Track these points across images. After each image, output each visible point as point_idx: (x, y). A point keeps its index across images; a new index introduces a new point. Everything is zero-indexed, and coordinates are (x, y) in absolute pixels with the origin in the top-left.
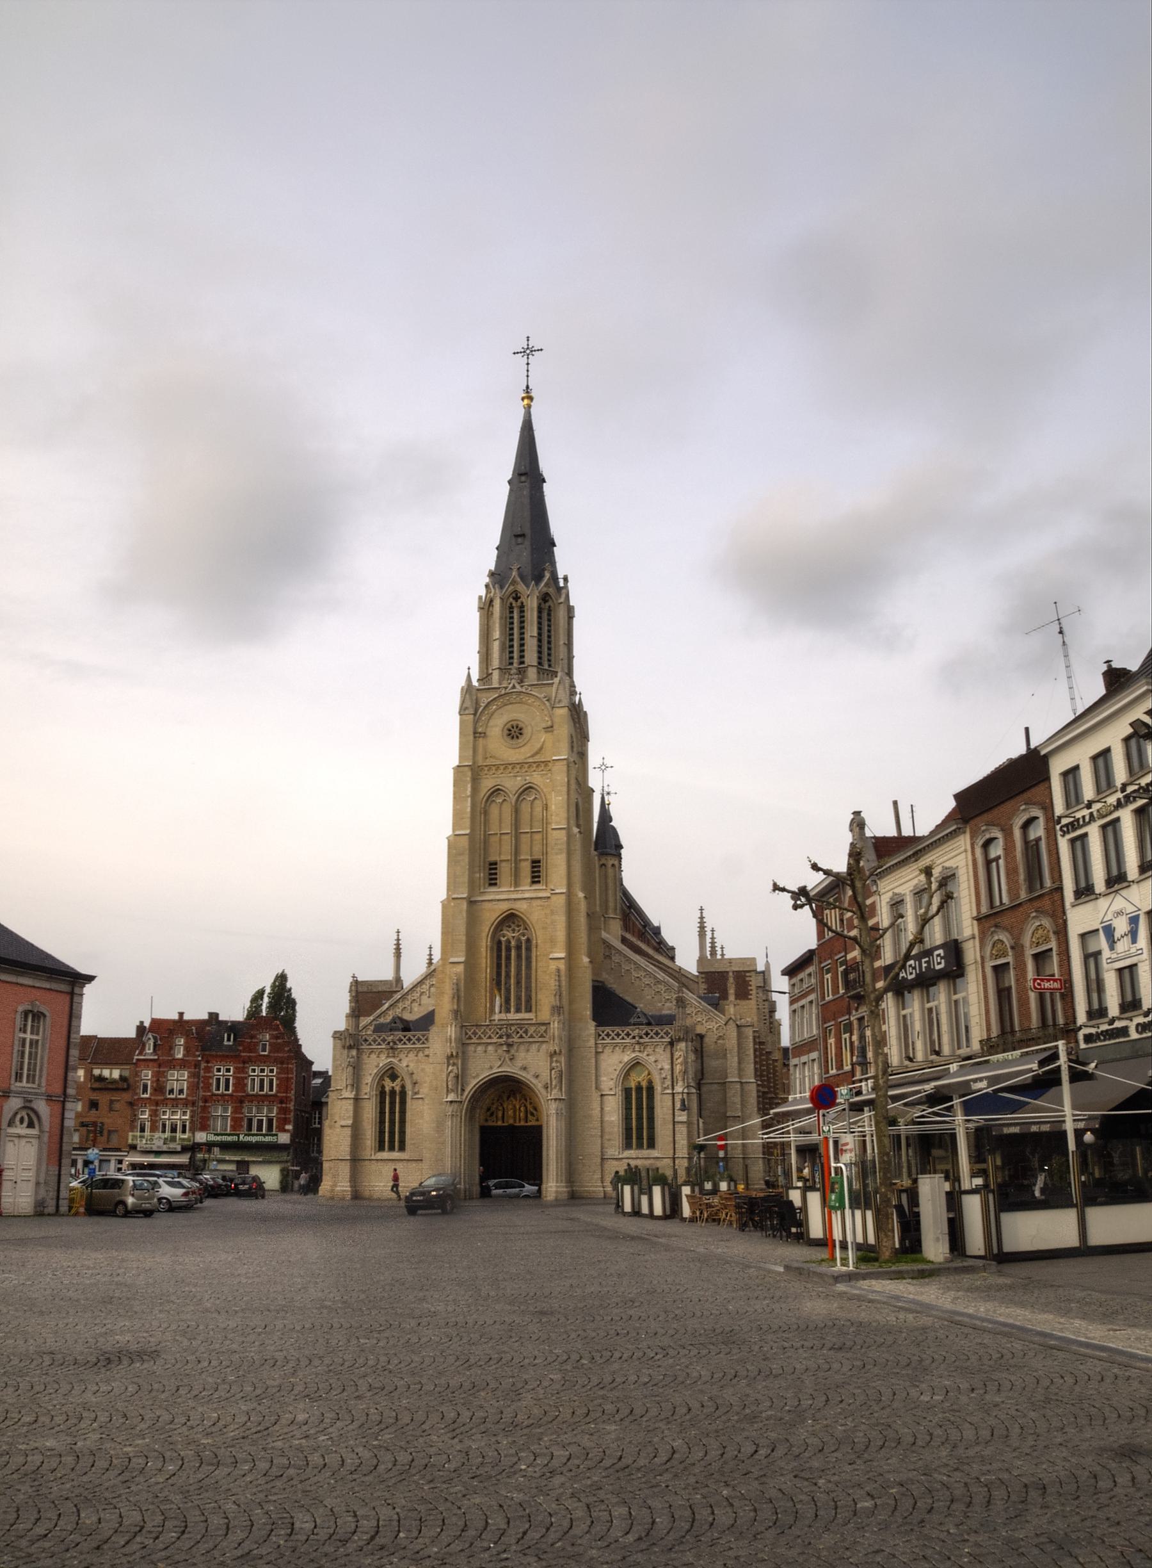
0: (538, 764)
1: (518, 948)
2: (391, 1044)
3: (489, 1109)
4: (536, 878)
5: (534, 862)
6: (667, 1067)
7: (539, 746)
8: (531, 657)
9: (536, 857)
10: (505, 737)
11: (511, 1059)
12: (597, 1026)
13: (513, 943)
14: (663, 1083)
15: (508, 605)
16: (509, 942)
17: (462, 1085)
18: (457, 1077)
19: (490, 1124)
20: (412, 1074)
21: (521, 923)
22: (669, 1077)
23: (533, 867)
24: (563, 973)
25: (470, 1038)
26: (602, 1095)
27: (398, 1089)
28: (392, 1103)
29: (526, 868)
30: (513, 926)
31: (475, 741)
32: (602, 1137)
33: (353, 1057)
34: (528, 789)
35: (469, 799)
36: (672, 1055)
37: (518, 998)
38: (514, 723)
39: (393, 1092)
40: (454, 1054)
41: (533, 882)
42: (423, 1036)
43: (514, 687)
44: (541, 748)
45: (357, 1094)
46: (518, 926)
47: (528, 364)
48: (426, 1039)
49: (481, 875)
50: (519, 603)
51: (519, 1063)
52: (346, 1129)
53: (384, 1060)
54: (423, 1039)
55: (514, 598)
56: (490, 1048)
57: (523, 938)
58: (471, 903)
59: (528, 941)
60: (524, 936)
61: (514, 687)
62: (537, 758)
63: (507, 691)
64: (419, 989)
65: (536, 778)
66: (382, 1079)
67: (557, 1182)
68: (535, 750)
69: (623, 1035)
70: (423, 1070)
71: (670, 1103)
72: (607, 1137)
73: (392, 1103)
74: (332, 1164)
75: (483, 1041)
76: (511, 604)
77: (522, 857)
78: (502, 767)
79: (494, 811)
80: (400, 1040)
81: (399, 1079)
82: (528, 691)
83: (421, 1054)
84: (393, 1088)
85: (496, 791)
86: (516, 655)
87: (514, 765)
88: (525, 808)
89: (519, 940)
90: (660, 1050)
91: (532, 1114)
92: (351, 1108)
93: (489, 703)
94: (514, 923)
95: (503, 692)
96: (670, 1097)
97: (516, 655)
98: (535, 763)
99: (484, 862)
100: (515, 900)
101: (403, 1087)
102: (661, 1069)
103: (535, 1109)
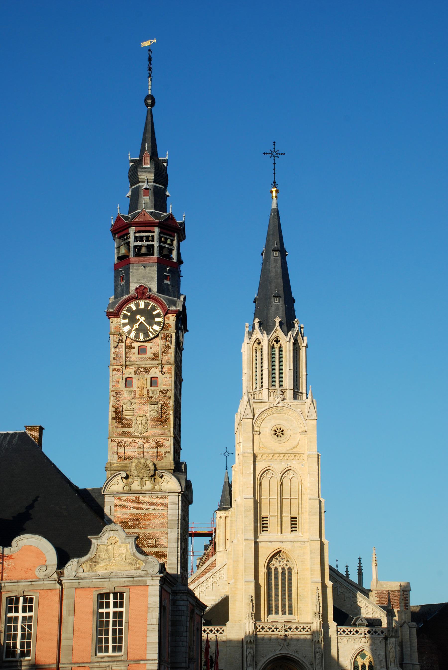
0: (295, 455)
1: (283, 573)
4: (293, 528)
6: (383, 653)
7: (296, 444)
8: (288, 382)
9: (294, 515)
10: (273, 435)
12: (337, 626)
13: (280, 570)
14: (380, 664)
16: (276, 569)
21: (285, 557)
22: (384, 660)
23: (292, 521)
30: (279, 559)
31: (405, 615)
37: (284, 605)
40: (252, 641)
43: (278, 403)
46: (282, 559)
47: (274, 164)
48: (223, 631)
50: (279, 345)
55: (275, 341)
57: (286, 568)
59: (290, 569)
62: (295, 451)
63: (275, 404)
65: (294, 465)
68: (294, 445)
76: (273, 345)
86: (277, 379)
87: (279, 454)
88: (286, 482)
89: (283, 569)
95: (272, 406)
97: (277, 379)
102: (379, 655)
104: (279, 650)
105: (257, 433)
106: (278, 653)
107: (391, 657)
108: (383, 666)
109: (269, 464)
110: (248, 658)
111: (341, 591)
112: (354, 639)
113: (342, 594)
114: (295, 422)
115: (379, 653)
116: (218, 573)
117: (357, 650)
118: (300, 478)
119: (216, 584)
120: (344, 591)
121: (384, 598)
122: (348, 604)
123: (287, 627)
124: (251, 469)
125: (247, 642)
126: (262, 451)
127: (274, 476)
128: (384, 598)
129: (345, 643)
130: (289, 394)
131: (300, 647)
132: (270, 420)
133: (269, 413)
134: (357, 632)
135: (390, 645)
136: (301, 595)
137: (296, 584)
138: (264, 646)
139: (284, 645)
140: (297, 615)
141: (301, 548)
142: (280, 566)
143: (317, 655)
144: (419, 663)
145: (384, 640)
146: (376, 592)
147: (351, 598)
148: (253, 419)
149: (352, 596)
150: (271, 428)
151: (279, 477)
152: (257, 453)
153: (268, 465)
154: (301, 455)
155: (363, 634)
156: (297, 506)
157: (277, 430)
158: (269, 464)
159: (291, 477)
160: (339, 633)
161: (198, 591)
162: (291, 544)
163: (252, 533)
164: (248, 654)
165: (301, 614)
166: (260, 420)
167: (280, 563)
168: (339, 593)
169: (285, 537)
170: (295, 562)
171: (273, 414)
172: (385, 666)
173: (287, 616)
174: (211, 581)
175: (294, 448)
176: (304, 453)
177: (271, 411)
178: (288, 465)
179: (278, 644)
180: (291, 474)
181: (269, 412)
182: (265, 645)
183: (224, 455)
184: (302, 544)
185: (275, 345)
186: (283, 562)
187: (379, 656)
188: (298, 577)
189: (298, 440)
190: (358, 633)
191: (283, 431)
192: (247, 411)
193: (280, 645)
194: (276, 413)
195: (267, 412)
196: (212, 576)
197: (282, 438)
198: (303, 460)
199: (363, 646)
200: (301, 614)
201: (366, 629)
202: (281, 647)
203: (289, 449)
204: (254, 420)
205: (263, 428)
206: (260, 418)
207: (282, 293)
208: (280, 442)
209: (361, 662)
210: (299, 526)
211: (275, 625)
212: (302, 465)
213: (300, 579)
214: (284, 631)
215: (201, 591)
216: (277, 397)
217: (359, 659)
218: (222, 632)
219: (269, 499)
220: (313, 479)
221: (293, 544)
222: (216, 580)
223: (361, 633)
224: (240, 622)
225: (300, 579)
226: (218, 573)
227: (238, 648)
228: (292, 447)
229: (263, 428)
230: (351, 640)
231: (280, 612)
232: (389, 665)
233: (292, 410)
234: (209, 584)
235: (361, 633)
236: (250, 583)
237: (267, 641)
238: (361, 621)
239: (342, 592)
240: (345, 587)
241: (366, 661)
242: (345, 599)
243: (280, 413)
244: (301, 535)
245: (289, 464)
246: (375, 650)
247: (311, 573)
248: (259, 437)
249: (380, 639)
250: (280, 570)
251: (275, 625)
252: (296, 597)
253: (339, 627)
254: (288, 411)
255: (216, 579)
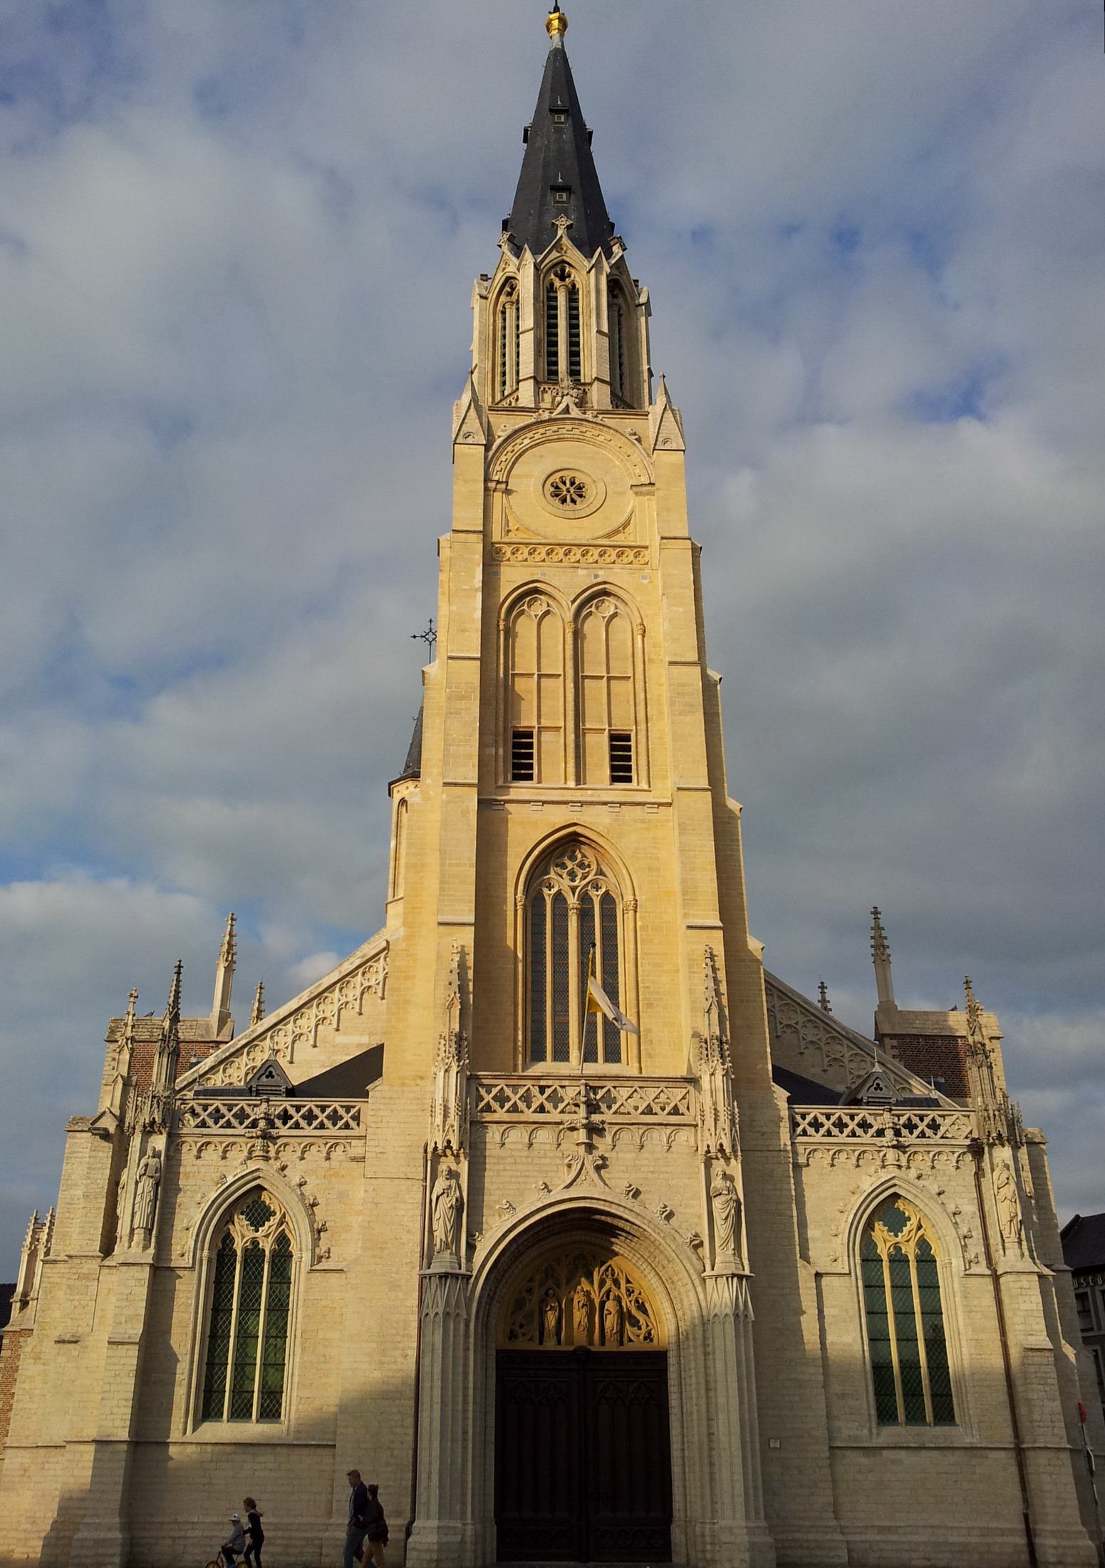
0: (621, 550)
1: (585, 915)
2: (262, 1124)
3: (519, 1304)
4: (621, 771)
5: (613, 737)
6: (970, 1208)
7: (623, 519)
8: (594, 361)
11: (598, 1169)
13: (572, 901)
15: (547, 284)
16: (559, 898)
17: (470, 1235)
18: (458, 1209)
19: (522, 1344)
20: (314, 1205)
22: (977, 1234)
24: (720, 962)
25: (488, 1108)
26: (818, 1276)
27: (267, 1246)
28: (251, 1283)
29: (599, 749)
30: (570, 865)
32: (826, 1386)
33: (156, 1155)
34: (600, 594)
35: (480, 595)
36: (979, 1174)
38: (568, 475)
39: (253, 1253)
41: (615, 779)
42: (348, 1109)
43: (567, 410)
44: (626, 525)
45: (157, 1256)
46: (581, 865)
48: (356, 1118)
49: (502, 752)
51: (619, 1179)
52: (122, 1350)
53: (236, 1167)
54: (347, 1117)
56: (543, 1136)
57: (596, 896)
58: (485, 805)
59: (607, 899)
60: (597, 888)
61: (567, 410)
62: (619, 539)
63: (553, 416)
64: (290, 1026)
65: (618, 576)
66: (227, 1218)
67: (747, 1517)
68: (615, 525)
69: (852, 1125)
70: (343, 1196)
71: (989, 1301)
72: (836, 1388)
73: (251, 1283)
74: (24, 1458)
75: (522, 1118)
76: (552, 285)
77: (588, 726)
78: (543, 550)
79: (525, 628)
80: (285, 1117)
81: (274, 1221)
82: (598, 420)
83: (338, 1154)
84: (255, 1242)
85: (531, 592)
87: (569, 547)
88: (594, 627)
89: (585, 899)
90: (947, 1162)
91: (635, 1323)
92: (142, 1292)
93: (516, 432)
94: (573, 858)
96: (988, 1284)
98: (614, 547)
99: (505, 728)
100: (583, 803)
101: (283, 1240)
103: (642, 1307)
104: (563, 1186)
105: (499, 486)
106: (558, 1198)
107: (1005, 1219)
108: (977, 1257)
109: (538, 574)
110: (436, 1217)
111: (785, 1022)
112: (857, 1153)
113: (789, 1031)
114: (617, 463)
115: (957, 1207)
116: (382, 959)
117: (869, 1195)
118: (638, 615)
119: (374, 996)
120: (796, 1024)
121: (921, 1061)
122: (813, 1066)
123: (595, 1094)
124: (474, 578)
125: (436, 1148)
126: (513, 537)
127: (555, 607)
128: (921, 1061)
129: (823, 1168)
130: (599, 396)
131: (650, 1176)
132: (542, 456)
133: (537, 436)
134: (864, 1125)
135: (996, 1174)
136: (648, 987)
137: (632, 946)
138: (505, 1170)
139: (583, 1164)
140: (636, 1059)
141: (644, 826)
142: (573, 889)
143: (717, 1203)
144: (1068, 1268)
145: (969, 1157)
146: (894, 1042)
147: (822, 1044)
148: (487, 447)
149: (823, 1039)
150: (544, 477)
151: (569, 609)
152: (500, 543)
153: (532, 574)
154: (639, 549)
155: (889, 1134)
156: (628, 702)
157: (561, 485)
158: (538, 574)
159: (607, 615)
160: (799, 1130)
161: (313, 1017)
162: (612, 810)
163: (473, 766)
164: (438, 1198)
165: (650, 1056)
166: (510, 455)
167: (573, 880)
168: (779, 1026)
169: (589, 792)
170: (625, 871)
171: (550, 441)
172: (982, 1259)
173: (600, 1067)
174: (358, 985)
175: (616, 532)
176: (647, 543)
177: (542, 431)
178: (596, 576)
179: (558, 1161)
180: (609, 607)
181: (538, 434)
182: (508, 1168)
183: (424, 639)
184: (650, 810)
185: (557, 283)
186: (586, 877)
187: (958, 1218)
188: (639, 923)
189: (630, 508)
190: (871, 1131)
191: (580, 488)
192: (469, 425)
193: (569, 1166)
194: (560, 439)
195: (531, 434)
196: (361, 970)
197: (578, 506)
198: (647, 564)
199: (894, 1177)
200: (650, 1056)
201: (899, 1116)
202: (573, 1174)
203: (601, 533)
204: (491, 454)
205: (519, 476)
206: (510, 448)
207: (575, 183)
208: (571, 515)
209: (888, 1244)
210: (638, 762)
211: (549, 1087)
212: (644, 578)
213: (644, 928)
214: (582, 1111)
215: (321, 1015)
216: (560, 394)
217: (881, 1233)
218: (353, 1124)
219: (536, 676)
220: (681, 610)
221: (617, 810)
222: (373, 982)
223: (883, 1130)
224: (419, 1081)
225: (644, 928)
226: (382, 959)
227: (409, 1182)
228: (608, 530)
229: (519, 476)
230: (843, 1156)
231: (574, 1053)
232: (1001, 1252)
233: (607, 430)
234: (352, 993)
235: (883, 1130)
236: (456, 927)
237: (520, 1150)
238: (876, 1089)
239: (789, 1026)
240: (799, 1010)
241: (908, 1241)
242: (803, 1047)
243: (572, 440)
244: (646, 787)
245: (600, 573)
246: (939, 1194)
247: (684, 900)
248: (504, 499)
249: (953, 1152)
250: (572, 901)
251: (549, 1087)
252: (631, 995)
253: (800, 1109)
254: (597, 433)
255: (374, 978)
